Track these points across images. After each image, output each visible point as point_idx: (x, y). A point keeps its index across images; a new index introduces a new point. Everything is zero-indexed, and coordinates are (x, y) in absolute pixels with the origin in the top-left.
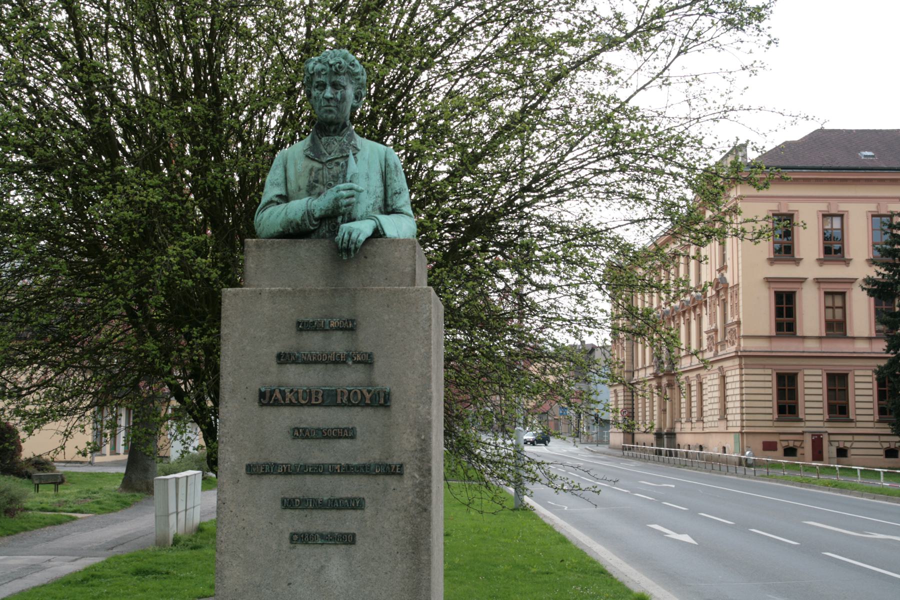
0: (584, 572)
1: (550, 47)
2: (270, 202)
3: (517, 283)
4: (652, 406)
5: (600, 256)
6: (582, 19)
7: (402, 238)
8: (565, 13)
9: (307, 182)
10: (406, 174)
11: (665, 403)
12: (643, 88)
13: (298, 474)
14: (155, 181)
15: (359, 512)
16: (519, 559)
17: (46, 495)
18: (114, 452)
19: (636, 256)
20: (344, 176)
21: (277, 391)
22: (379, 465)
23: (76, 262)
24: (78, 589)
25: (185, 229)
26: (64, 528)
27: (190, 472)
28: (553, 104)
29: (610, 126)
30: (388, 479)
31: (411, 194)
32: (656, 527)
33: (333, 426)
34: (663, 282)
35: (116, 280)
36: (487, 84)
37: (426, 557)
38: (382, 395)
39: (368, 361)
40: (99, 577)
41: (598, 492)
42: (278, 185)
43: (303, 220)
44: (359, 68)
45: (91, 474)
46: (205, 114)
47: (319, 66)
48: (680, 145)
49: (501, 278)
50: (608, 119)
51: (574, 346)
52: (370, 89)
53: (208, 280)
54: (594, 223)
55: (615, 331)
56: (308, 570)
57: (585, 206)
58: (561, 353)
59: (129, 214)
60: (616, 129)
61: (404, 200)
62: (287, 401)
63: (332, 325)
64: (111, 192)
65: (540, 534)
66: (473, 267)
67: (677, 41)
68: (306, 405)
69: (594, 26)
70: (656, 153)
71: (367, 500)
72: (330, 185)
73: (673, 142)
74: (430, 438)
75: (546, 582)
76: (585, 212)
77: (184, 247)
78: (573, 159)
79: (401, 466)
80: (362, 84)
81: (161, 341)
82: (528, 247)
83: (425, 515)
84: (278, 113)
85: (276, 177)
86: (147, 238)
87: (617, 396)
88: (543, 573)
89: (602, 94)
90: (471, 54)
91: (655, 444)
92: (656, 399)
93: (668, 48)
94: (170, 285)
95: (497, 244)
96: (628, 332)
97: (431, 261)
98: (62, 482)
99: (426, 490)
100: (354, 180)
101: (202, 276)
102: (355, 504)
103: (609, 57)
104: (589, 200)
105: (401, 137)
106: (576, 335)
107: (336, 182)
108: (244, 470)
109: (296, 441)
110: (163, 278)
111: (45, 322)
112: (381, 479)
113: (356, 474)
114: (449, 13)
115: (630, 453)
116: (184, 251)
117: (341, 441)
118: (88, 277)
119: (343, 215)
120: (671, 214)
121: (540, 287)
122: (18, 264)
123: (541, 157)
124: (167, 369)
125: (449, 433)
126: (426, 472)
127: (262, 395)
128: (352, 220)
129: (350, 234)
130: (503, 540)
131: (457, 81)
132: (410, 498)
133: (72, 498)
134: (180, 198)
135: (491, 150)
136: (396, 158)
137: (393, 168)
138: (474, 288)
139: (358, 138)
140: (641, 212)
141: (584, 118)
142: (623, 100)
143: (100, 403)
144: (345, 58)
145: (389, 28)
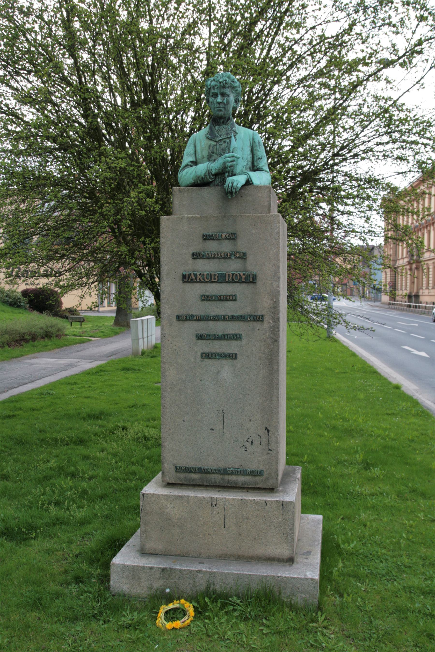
0: (365, 372)
1: (352, 67)
2: (187, 166)
3: (330, 210)
4: (406, 280)
5: (378, 194)
6: (371, 48)
7: (262, 185)
8: (361, 45)
9: (207, 153)
10: (266, 147)
11: (414, 280)
12: (408, 91)
13: (205, 320)
14: (123, 155)
15: (239, 342)
16: (328, 365)
17: (75, 328)
18: (109, 305)
19: (400, 194)
20: (229, 149)
21: (192, 274)
22: (250, 316)
23: (83, 202)
24: (94, 377)
25: (140, 182)
26: (86, 345)
27: (149, 317)
28: (353, 103)
29: (387, 115)
30: (255, 323)
31: (268, 159)
32: (406, 348)
33: (224, 294)
34: (416, 210)
35: (103, 212)
36: (313, 92)
37: (276, 367)
38: (251, 276)
39: (243, 257)
40: (104, 371)
41: (374, 331)
42: (191, 155)
43: (205, 176)
44: (237, 84)
45: (98, 317)
46: (149, 115)
47: (213, 83)
48: (429, 126)
49: (321, 207)
50: (386, 111)
51: (362, 246)
52: (244, 97)
53: (154, 211)
54: (376, 175)
55: (386, 239)
56: (211, 372)
57: (370, 164)
58: (355, 250)
59: (108, 174)
60: (391, 117)
61: (264, 163)
62: (198, 280)
63: (223, 236)
64: (98, 162)
65: (341, 351)
66: (304, 201)
67: (429, 61)
68: (208, 282)
69: (378, 52)
70: (414, 131)
71: (243, 335)
72: (221, 155)
73: (425, 124)
74: (279, 301)
75: (343, 378)
76: (371, 168)
77: (139, 193)
78: (364, 136)
79: (262, 316)
80: (239, 93)
81: (129, 246)
82: (337, 190)
83: (276, 343)
84: (191, 113)
85: (190, 151)
86: (119, 187)
87: (386, 274)
88: (342, 373)
89: (382, 96)
90: (303, 73)
91: (407, 301)
92: (409, 276)
93: (424, 65)
94: (133, 214)
95: (319, 188)
96: (394, 239)
97: (280, 198)
98: (84, 321)
99: (277, 330)
100: (235, 151)
101: (150, 209)
102: (237, 337)
103: (386, 72)
104: (373, 161)
105: (262, 125)
106: (364, 240)
107: (224, 153)
108: (175, 318)
109: (203, 302)
110: (129, 211)
111: (67, 236)
112: (251, 323)
113: (237, 320)
114: (290, 48)
115: (393, 306)
116: (139, 195)
117: (229, 302)
118: (89, 211)
119: (229, 172)
120: (422, 168)
121: (343, 213)
122: (53, 203)
123: (345, 135)
124: (133, 261)
125: (290, 297)
126: (277, 320)
127: (184, 276)
128: (233, 175)
129: (232, 184)
130: (320, 354)
131: (295, 90)
132: (268, 334)
133: (89, 330)
134: (137, 164)
135: (316, 132)
136: (260, 138)
137: (257, 144)
138: (305, 214)
139: (237, 126)
140: (404, 167)
141: (371, 111)
142: (395, 99)
143: (101, 281)
144: (229, 77)
145: (255, 59)
